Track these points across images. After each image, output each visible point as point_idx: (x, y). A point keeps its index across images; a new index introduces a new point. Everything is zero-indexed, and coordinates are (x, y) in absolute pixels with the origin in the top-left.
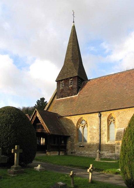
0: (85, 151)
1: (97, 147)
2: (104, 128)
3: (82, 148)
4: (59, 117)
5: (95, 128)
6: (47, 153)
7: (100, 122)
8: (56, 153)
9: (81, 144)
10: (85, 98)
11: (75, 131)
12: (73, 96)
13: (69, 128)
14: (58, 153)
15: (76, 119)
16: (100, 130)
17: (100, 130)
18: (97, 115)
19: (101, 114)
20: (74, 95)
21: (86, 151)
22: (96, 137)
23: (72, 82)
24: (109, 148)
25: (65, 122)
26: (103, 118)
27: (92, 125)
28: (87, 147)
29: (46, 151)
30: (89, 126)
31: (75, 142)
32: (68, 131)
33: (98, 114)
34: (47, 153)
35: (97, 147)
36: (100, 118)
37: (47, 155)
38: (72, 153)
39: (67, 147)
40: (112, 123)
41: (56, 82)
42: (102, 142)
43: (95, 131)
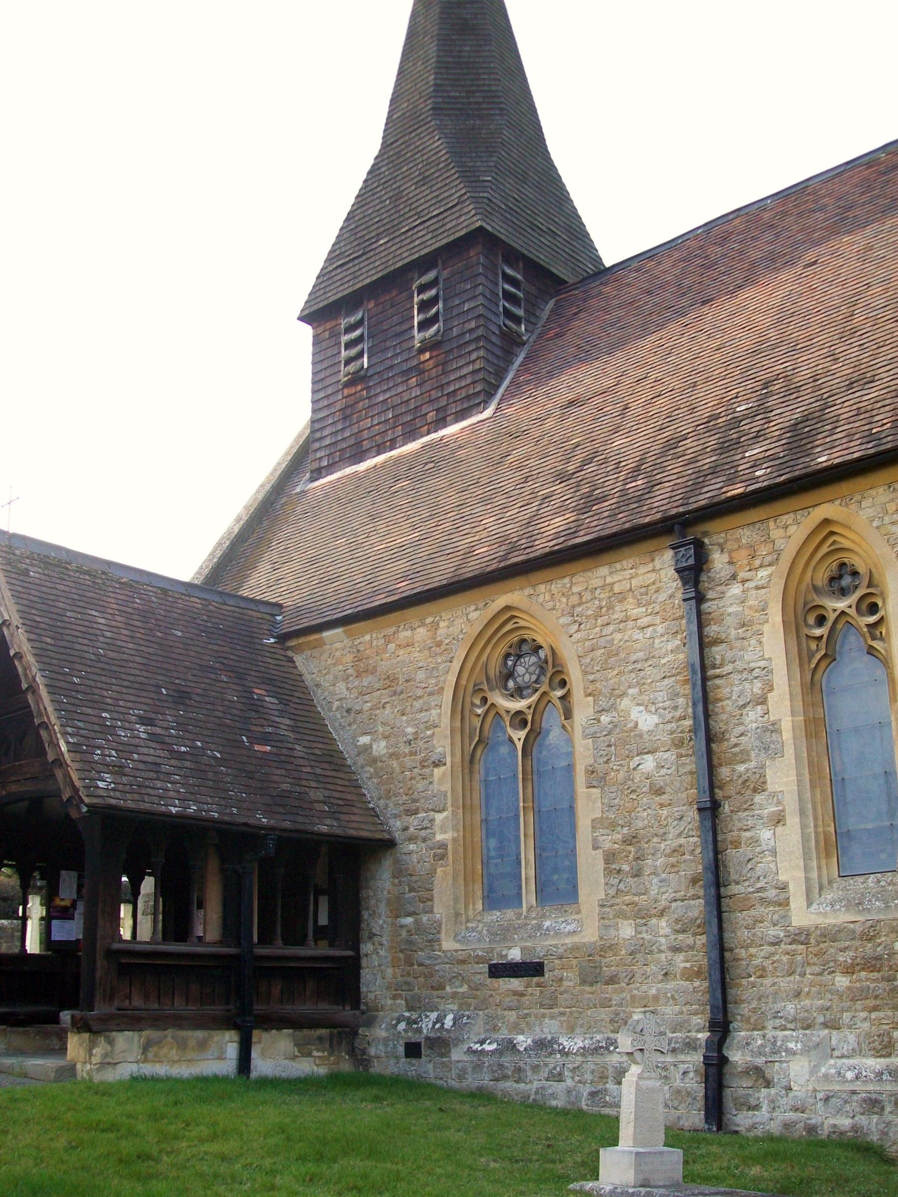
0: (549, 1028)
1: (688, 975)
2: (753, 717)
3: (515, 984)
4: (283, 638)
5: (646, 721)
6: (75, 1044)
7: (704, 643)
8: (202, 1046)
9: (504, 933)
10: (550, 423)
11: (438, 772)
12: (452, 429)
13: (380, 748)
14: (232, 1050)
15: (442, 632)
16: (710, 738)
17: (710, 738)
18: (722, 900)
19: (699, 546)
20: (462, 415)
21: (571, 1030)
22: (672, 842)
23: (434, 301)
24: (842, 981)
25: (341, 687)
26: (736, 590)
27: (617, 694)
28: (571, 979)
29: (66, 1016)
30: (583, 711)
31: (440, 910)
32: (371, 789)
33: (669, 554)
34: (75, 1044)
35: (688, 975)
36: (700, 599)
37: (72, 1069)
38: (413, 1050)
39: (366, 975)
40: (852, 643)
41: (307, 331)
42: (708, 636)
43: (649, 763)
